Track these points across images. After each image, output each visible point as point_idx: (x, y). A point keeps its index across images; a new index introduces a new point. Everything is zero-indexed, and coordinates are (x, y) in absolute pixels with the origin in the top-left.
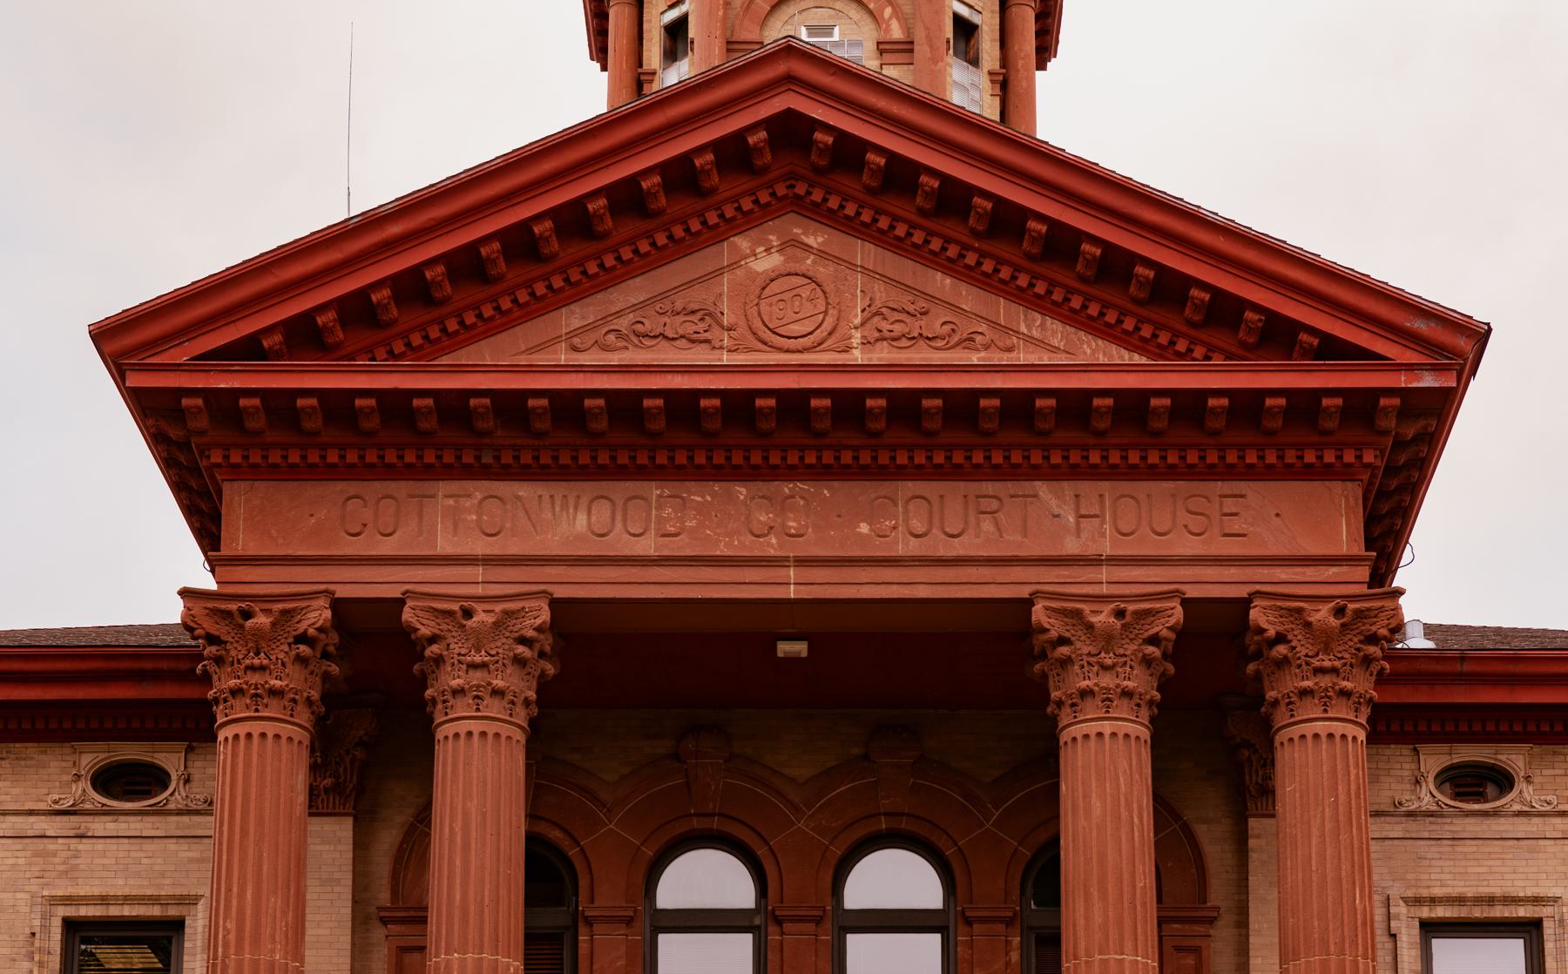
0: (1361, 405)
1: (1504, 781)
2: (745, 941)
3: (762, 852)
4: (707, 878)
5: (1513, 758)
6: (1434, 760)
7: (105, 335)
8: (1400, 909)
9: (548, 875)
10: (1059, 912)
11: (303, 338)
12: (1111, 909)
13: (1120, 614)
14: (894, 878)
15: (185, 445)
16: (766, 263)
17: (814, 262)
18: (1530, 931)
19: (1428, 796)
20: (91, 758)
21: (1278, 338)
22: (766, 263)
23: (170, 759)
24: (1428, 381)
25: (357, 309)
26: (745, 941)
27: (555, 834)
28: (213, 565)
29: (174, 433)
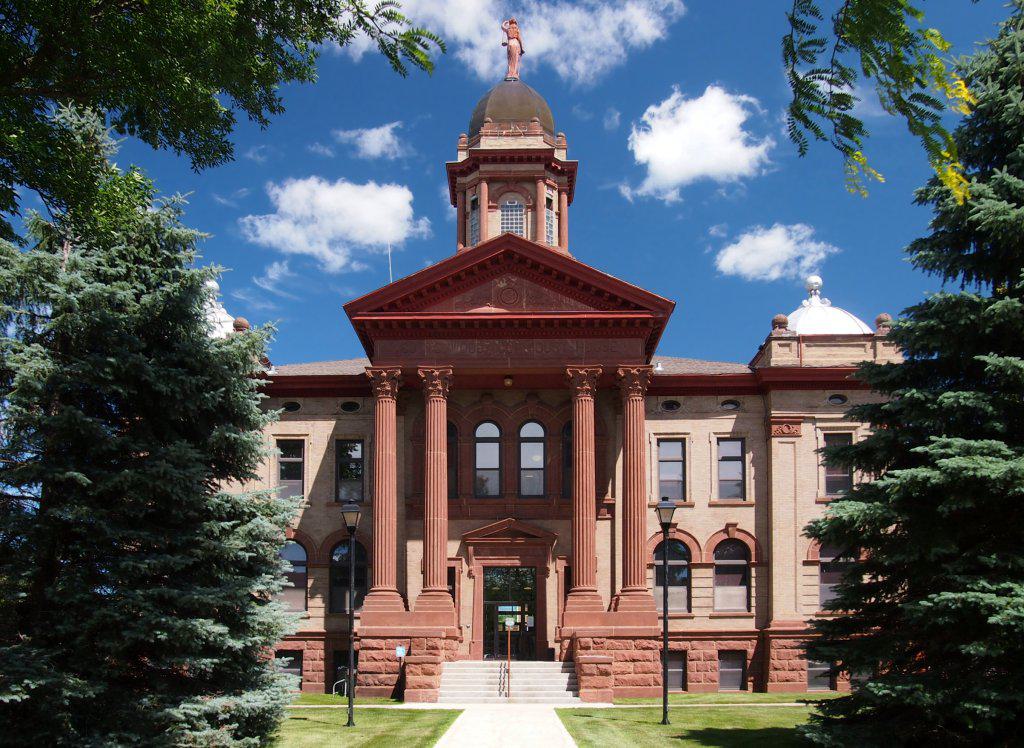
0: (644, 322)
1: (678, 405)
2: (496, 446)
3: (499, 421)
4: (487, 430)
5: (680, 399)
6: (662, 399)
7: (346, 308)
8: (652, 436)
9: (452, 430)
10: (736, 585)
11: (393, 307)
12: (753, 590)
13: (587, 371)
14: (532, 430)
15: (508, 573)
16: (502, 285)
17: (1007, 566)
18: (683, 441)
19: (660, 408)
20: (341, 400)
21: (626, 305)
22: (502, 285)
23: (358, 400)
24: (661, 316)
25: (405, 300)
26: (496, 446)
27: (454, 422)
28: (371, 362)
29: (362, 329)
